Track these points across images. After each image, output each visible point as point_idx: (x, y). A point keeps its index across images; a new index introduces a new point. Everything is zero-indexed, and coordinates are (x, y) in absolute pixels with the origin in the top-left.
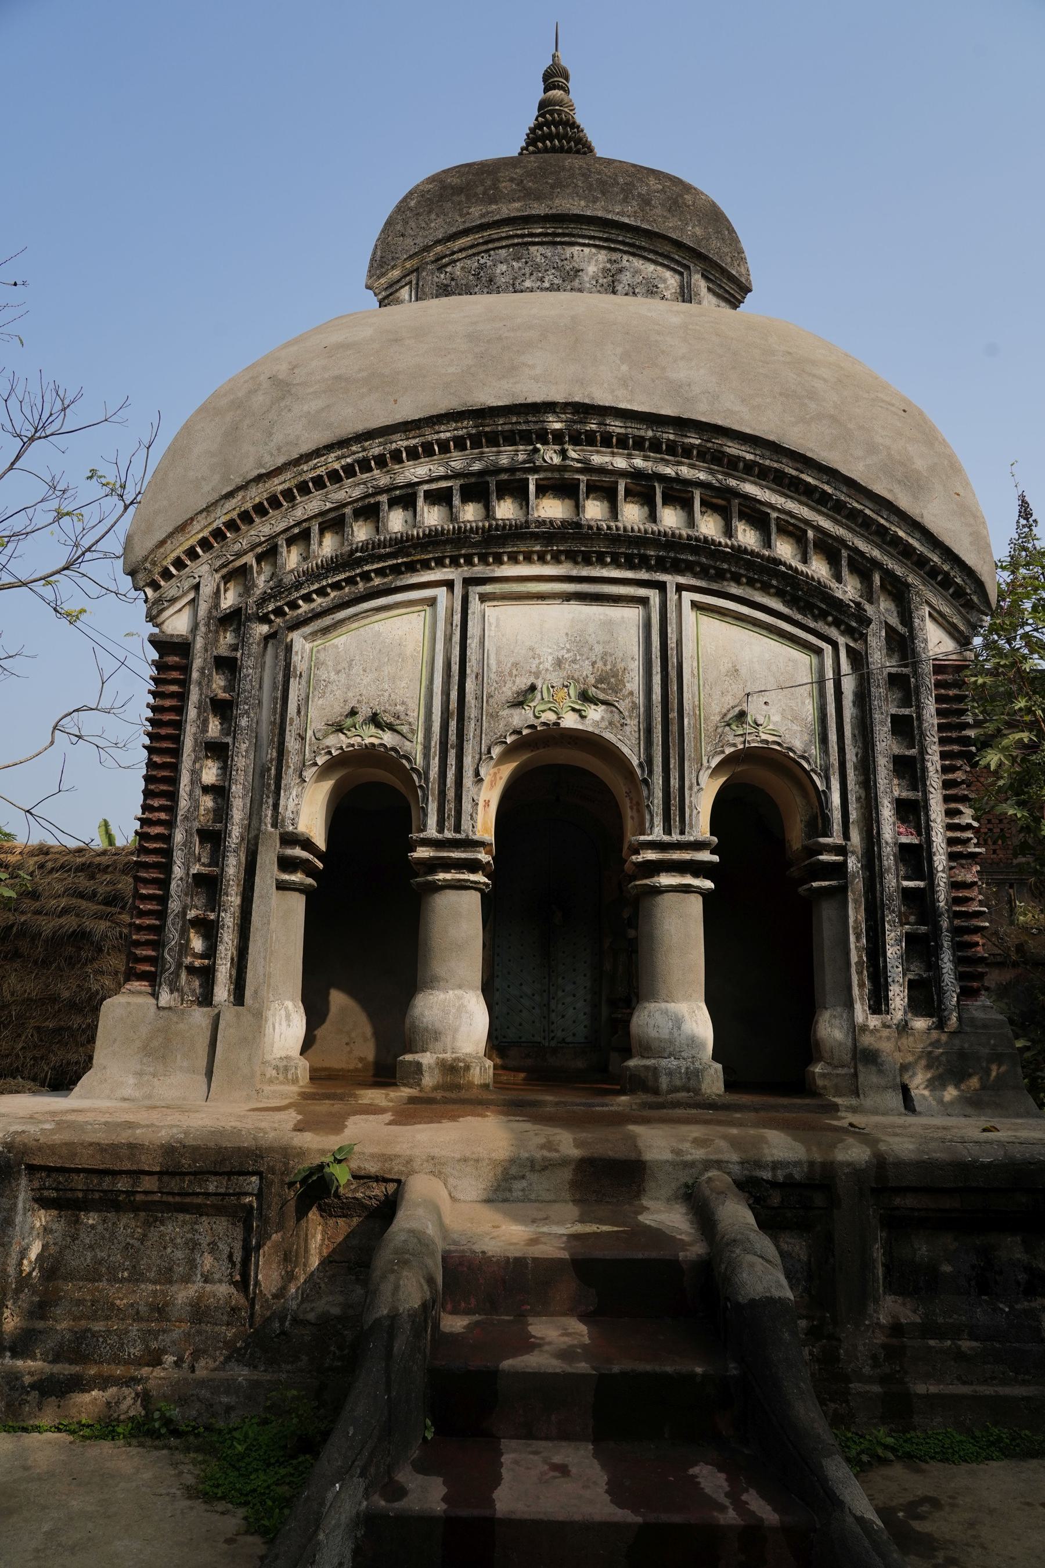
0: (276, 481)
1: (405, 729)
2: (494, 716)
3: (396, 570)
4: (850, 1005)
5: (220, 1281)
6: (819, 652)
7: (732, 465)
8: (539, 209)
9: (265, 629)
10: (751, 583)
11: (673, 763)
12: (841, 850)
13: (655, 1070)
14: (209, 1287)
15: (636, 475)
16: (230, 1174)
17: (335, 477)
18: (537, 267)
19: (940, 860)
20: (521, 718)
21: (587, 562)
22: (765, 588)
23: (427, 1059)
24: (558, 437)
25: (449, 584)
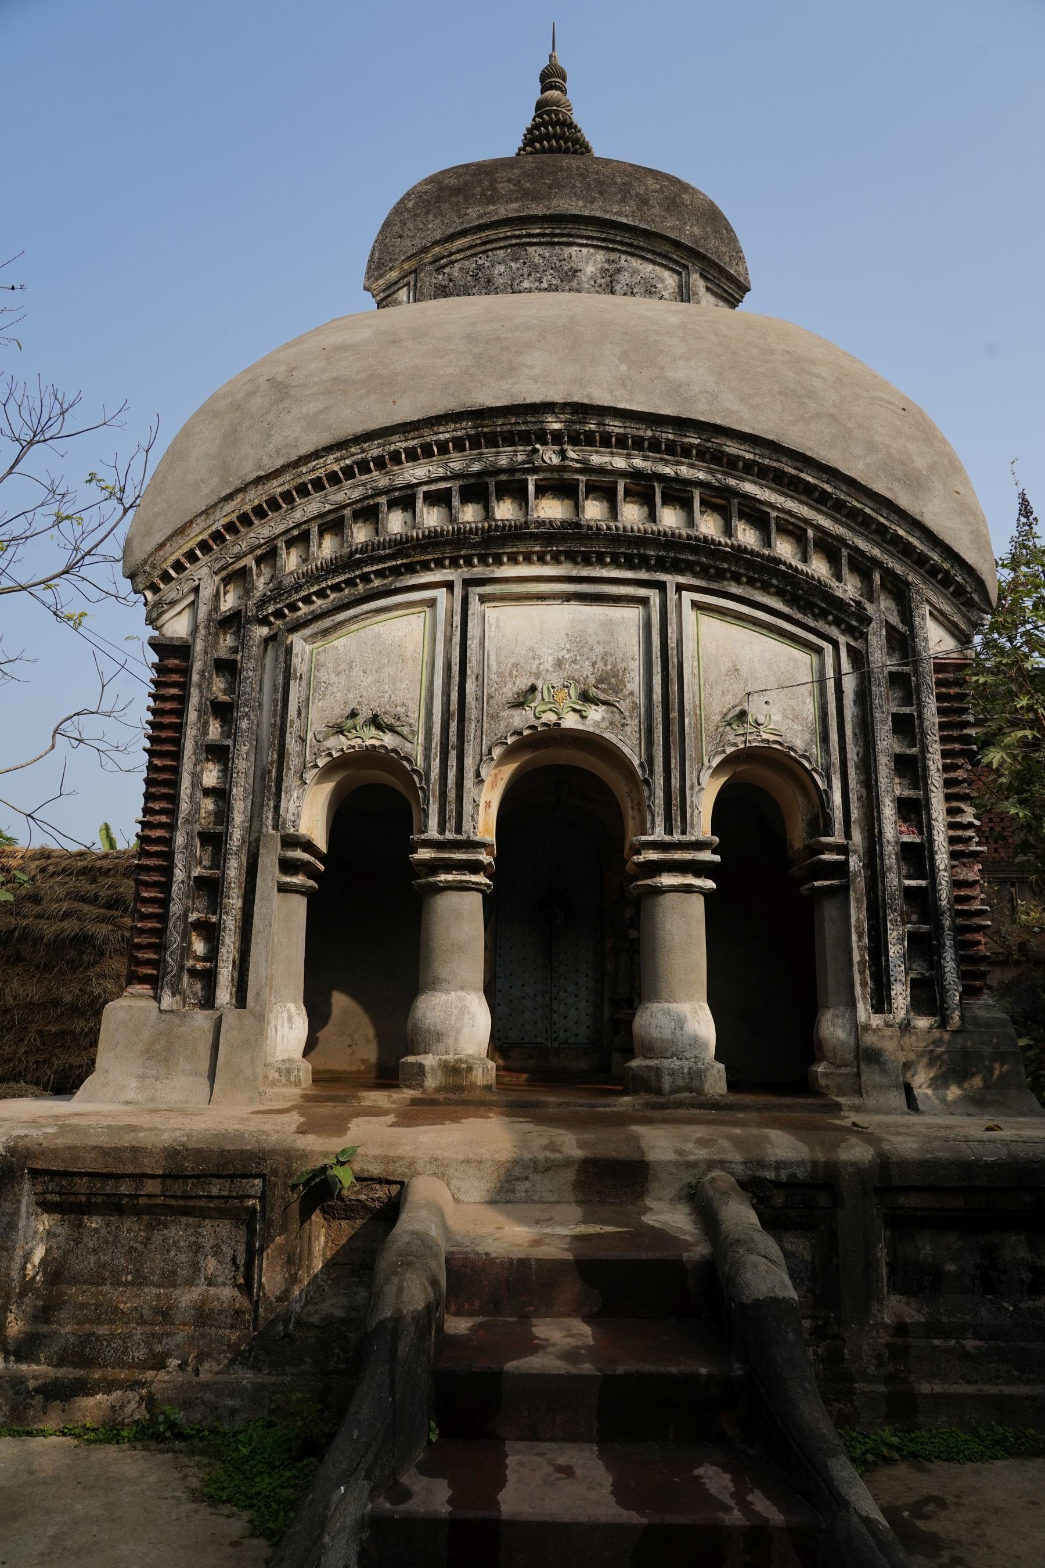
0: (275, 483)
1: (405, 730)
2: (495, 717)
3: (396, 571)
4: (852, 1005)
5: (224, 1284)
6: (819, 651)
7: (731, 464)
8: (537, 209)
9: (265, 631)
10: (751, 582)
11: (674, 762)
12: (843, 849)
13: (657, 1070)
14: (212, 1290)
15: (636, 475)
16: (232, 1177)
17: (334, 478)
18: (535, 268)
19: (942, 859)
20: (521, 719)
21: (587, 562)
22: (765, 588)
23: (429, 1060)
24: (557, 438)
25: (449, 585)
